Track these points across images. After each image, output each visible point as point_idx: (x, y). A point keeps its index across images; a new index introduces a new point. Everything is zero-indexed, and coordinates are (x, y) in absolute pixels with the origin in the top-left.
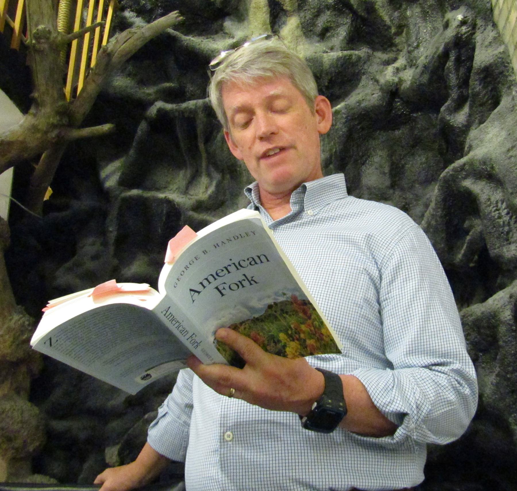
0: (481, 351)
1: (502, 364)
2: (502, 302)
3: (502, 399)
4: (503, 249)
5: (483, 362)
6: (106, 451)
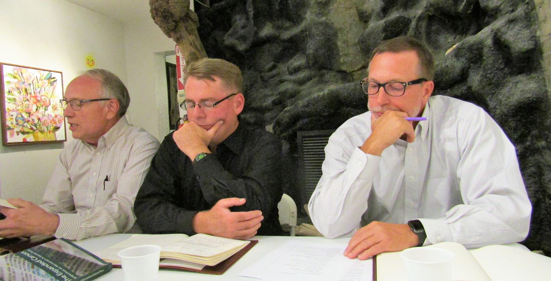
0: (472, 62)
1: (485, 70)
2: (487, 34)
3: (483, 88)
4: (488, 3)
5: (473, 69)
6: (266, 127)
